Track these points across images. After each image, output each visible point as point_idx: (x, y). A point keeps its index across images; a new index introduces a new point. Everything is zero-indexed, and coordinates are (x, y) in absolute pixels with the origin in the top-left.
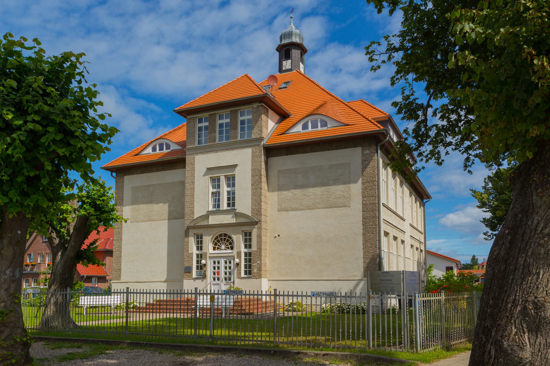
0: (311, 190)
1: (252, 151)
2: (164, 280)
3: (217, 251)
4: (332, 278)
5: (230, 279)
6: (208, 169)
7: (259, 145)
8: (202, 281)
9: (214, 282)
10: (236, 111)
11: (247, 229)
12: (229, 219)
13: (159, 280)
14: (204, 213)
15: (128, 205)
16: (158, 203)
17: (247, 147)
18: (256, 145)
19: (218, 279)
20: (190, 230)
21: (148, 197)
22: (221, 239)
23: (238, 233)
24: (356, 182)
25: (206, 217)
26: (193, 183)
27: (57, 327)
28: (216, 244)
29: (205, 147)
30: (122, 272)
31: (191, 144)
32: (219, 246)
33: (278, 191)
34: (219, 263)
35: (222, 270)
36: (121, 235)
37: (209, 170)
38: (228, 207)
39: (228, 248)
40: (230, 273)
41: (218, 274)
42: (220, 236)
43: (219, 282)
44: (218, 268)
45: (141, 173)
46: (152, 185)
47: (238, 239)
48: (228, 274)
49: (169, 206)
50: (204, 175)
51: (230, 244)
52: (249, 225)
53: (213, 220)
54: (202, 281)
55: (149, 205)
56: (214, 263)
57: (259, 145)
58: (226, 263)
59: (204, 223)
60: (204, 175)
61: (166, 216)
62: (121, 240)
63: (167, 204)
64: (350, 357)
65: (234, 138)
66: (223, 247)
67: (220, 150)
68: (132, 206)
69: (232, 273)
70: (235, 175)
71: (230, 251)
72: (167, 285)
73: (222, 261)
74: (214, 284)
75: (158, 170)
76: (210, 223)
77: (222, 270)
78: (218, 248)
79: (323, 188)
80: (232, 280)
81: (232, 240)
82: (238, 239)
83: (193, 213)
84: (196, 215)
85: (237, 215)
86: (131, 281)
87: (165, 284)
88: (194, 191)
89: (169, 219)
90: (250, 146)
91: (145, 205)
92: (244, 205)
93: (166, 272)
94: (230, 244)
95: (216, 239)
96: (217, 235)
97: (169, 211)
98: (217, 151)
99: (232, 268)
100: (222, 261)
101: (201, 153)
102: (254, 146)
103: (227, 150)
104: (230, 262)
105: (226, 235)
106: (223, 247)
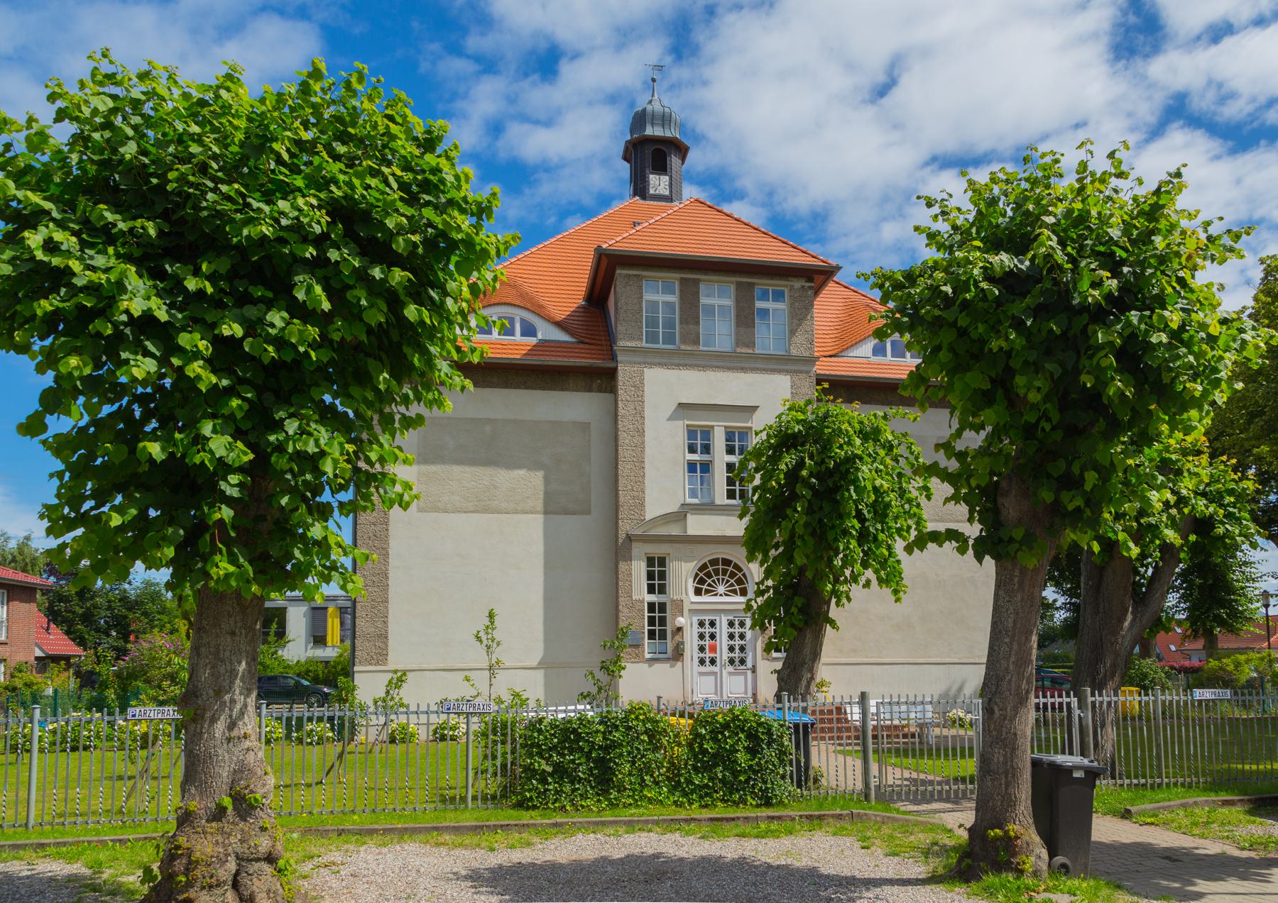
1: (793, 382)
2: (535, 664)
3: (705, 598)
4: (947, 660)
5: (742, 662)
7: (808, 372)
9: (703, 669)
10: (754, 284)
13: (520, 664)
14: (673, 507)
16: (511, 466)
17: (779, 371)
18: (801, 372)
19: (713, 662)
20: (634, 545)
25: (680, 516)
27: (1107, 884)
28: (702, 581)
29: (678, 353)
30: (391, 643)
31: (632, 338)
32: (709, 585)
34: (712, 624)
35: (723, 642)
36: (387, 542)
37: (685, 408)
38: (728, 497)
39: (734, 592)
40: (742, 649)
41: (713, 649)
42: (714, 562)
43: (713, 668)
44: (713, 636)
46: (489, 421)
48: (737, 650)
49: (547, 480)
50: (670, 419)
53: (698, 525)
55: (479, 470)
56: (701, 624)
57: (808, 372)
58: (731, 624)
59: (674, 530)
60: (670, 419)
61: (540, 505)
63: (540, 474)
64: (899, 794)
65: (748, 346)
67: (691, 366)
68: (424, 468)
69: (748, 649)
72: (546, 676)
73: (723, 621)
74: (701, 674)
75: (506, 385)
76: (691, 532)
77: (723, 642)
78: (707, 592)
80: (749, 664)
81: (744, 575)
83: (642, 505)
84: (652, 512)
86: (424, 666)
87: (540, 674)
88: (643, 452)
89: (546, 512)
90: (787, 372)
91: (467, 469)
93: (541, 645)
94: (739, 582)
95: (701, 569)
96: (706, 560)
97: (546, 493)
98: (704, 367)
100: (723, 621)
101: (660, 365)
102: (795, 371)
103: (729, 369)
105: (727, 562)
106: (721, 589)
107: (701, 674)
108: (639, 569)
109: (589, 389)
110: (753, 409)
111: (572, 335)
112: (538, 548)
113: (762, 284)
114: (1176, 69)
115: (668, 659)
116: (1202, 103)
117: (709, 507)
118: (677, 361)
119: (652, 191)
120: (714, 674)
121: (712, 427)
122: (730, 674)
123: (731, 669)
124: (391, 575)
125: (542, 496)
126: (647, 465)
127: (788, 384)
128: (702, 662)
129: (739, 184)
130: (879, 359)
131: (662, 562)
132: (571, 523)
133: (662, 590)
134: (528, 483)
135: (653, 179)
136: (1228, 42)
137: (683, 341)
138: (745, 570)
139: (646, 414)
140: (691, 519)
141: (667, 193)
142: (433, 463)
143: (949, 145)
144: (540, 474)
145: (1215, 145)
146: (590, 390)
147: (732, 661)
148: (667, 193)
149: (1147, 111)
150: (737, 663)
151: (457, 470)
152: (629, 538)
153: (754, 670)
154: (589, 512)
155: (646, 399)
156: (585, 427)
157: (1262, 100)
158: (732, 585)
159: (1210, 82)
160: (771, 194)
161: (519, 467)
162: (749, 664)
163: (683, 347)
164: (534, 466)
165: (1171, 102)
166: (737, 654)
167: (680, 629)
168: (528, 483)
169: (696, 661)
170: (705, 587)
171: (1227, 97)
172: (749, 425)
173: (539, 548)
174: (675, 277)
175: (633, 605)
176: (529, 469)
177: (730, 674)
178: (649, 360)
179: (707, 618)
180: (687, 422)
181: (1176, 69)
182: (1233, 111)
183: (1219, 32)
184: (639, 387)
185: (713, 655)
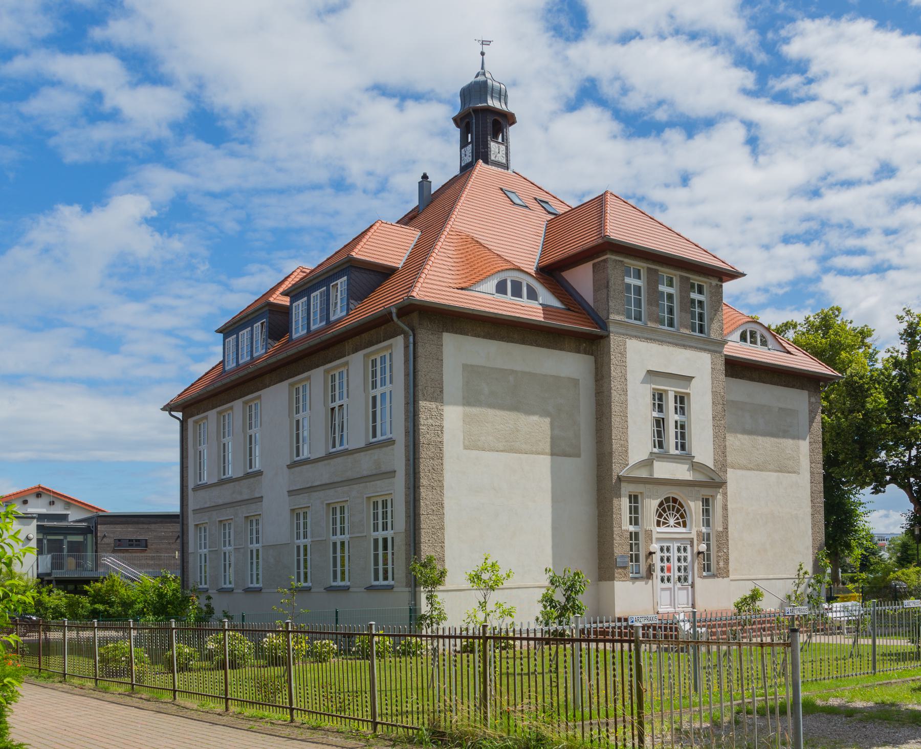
0: (760, 439)
5: (686, 579)
6: (649, 372)
8: (646, 584)
11: (706, 492)
12: (681, 472)
14: (645, 456)
15: (455, 404)
16: (529, 412)
17: (705, 350)
19: (669, 580)
20: (623, 485)
21: (513, 396)
22: (668, 507)
23: (697, 499)
24: (805, 439)
25: (648, 463)
26: (625, 392)
28: (660, 516)
33: (464, 405)
34: (668, 550)
35: (675, 564)
36: (442, 475)
39: (679, 524)
40: (685, 569)
42: (667, 500)
43: (670, 585)
45: (484, 337)
46: (513, 372)
47: (694, 507)
51: (682, 516)
52: (711, 484)
54: (646, 584)
58: (679, 550)
59: (643, 474)
61: (548, 450)
62: (442, 487)
63: (548, 420)
66: (672, 521)
70: (688, 394)
71: (681, 529)
74: (663, 589)
75: (787, 385)
76: (657, 475)
77: (675, 564)
78: (664, 523)
79: (773, 439)
82: (694, 507)
85: (696, 467)
90: (709, 351)
92: (703, 449)
94: (682, 516)
98: (662, 342)
99: (689, 559)
101: (636, 337)
104: (685, 550)
105: (675, 500)
106: (672, 521)
107: (663, 589)
108: (624, 504)
109: (578, 351)
110: (690, 379)
111: (562, 302)
112: (547, 483)
113: (665, 272)
114: (592, 57)
115: (642, 578)
116: (609, 90)
117: (666, 457)
118: (646, 336)
119: (493, 158)
120: (669, 589)
121: (666, 391)
122: (679, 589)
123: (679, 585)
124: (445, 505)
125: (549, 440)
126: (629, 420)
127: (709, 362)
128: (662, 580)
129: (165, 69)
130: (500, 297)
131: (636, 497)
132: (569, 463)
133: (636, 523)
134: (537, 427)
135: (493, 146)
136: (635, 45)
137: (635, 319)
138: (686, 508)
139: (629, 377)
140: (657, 464)
141: (504, 161)
142: (474, 406)
143: (393, 79)
144: (548, 420)
145: (616, 127)
146: (578, 352)
147: (679, 579)
148: (504, 161)
149: (569, 89)
150: (682, 580)
151: (490, 413)
152: (619, 479)
153: (693, 586)
154: (579, 456)
155: (628, 364)
156: (576, 382)
157: (653, 100)
158: (678, 519)
159: (617, 78)
160: (201, 86)
161: (534, 414)
162: (690, 582)
163: (650, 324)
164: (544, 413)
165: (587, 84)
166: (682, 574)
167: (651, 553)
168: (537, 427)
169: (659, 578)
170: (662, 520)
171: (625, 91)
172: (688, 391)
173: (547, 484)
174: (642, 265)
175: (623, 532)
176: (541, 416)
177: (679, 589)
178: (629, 333)
179: (665, 545)
180: (653, 386)
181: (592, 57)
182: (633, 102)
183: (627, 38)
184: (623, 354)
185: (668, 574)
